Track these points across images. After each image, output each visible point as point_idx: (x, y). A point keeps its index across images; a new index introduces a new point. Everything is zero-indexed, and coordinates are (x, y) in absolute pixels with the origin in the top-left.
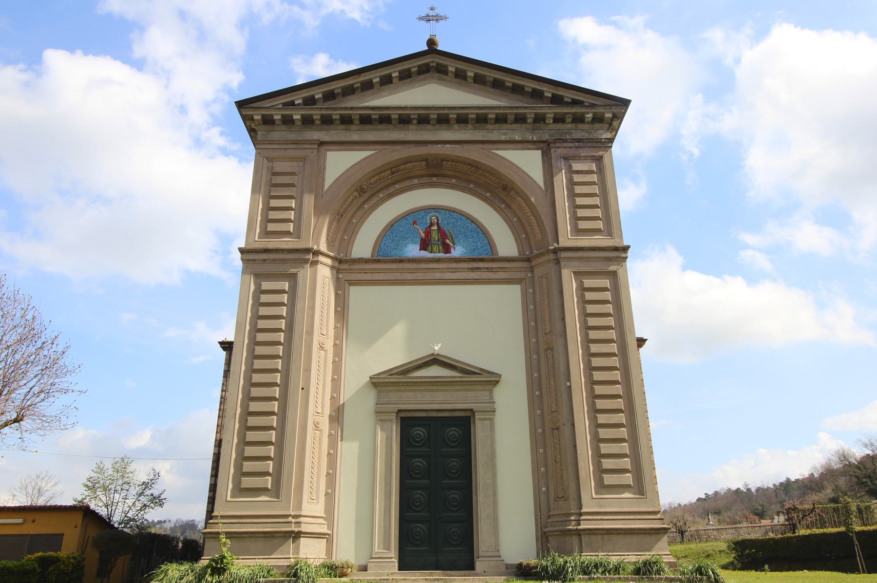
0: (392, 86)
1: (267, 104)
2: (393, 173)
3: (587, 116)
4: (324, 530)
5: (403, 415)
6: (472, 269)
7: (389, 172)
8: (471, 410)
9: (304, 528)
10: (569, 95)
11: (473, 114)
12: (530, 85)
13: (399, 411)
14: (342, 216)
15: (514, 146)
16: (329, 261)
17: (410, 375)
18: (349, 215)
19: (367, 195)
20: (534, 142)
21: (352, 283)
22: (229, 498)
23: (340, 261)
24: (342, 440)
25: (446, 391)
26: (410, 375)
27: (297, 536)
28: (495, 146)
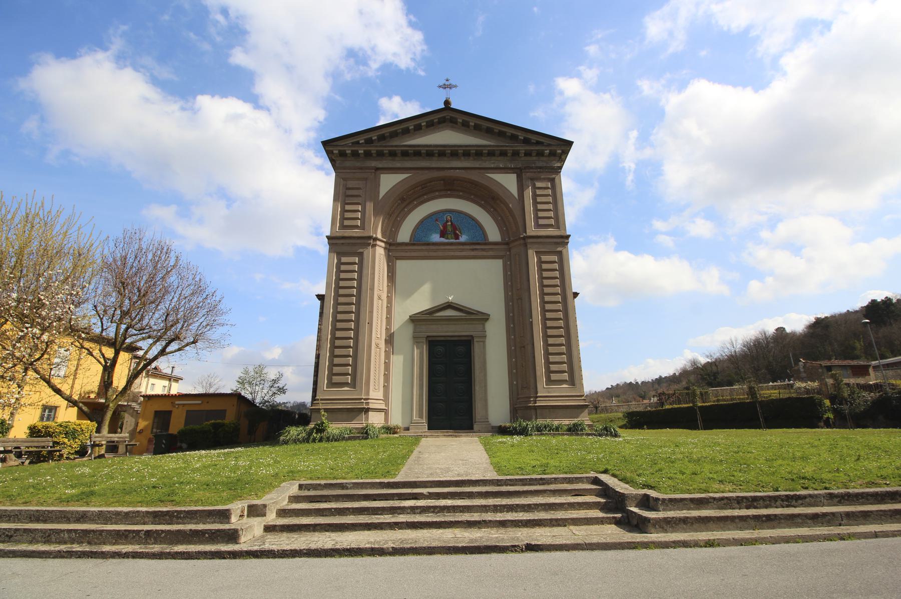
2: (423, 188)
3: (546, 152)
4: (384, 408)
5: (430, 339)
6: (473, 250)
9: (371, 406)
10: (534, 138)
13: (428, 337)
16: (383, 244)
22: (325, 389)
24: (393, 354)
25: (448, 324)
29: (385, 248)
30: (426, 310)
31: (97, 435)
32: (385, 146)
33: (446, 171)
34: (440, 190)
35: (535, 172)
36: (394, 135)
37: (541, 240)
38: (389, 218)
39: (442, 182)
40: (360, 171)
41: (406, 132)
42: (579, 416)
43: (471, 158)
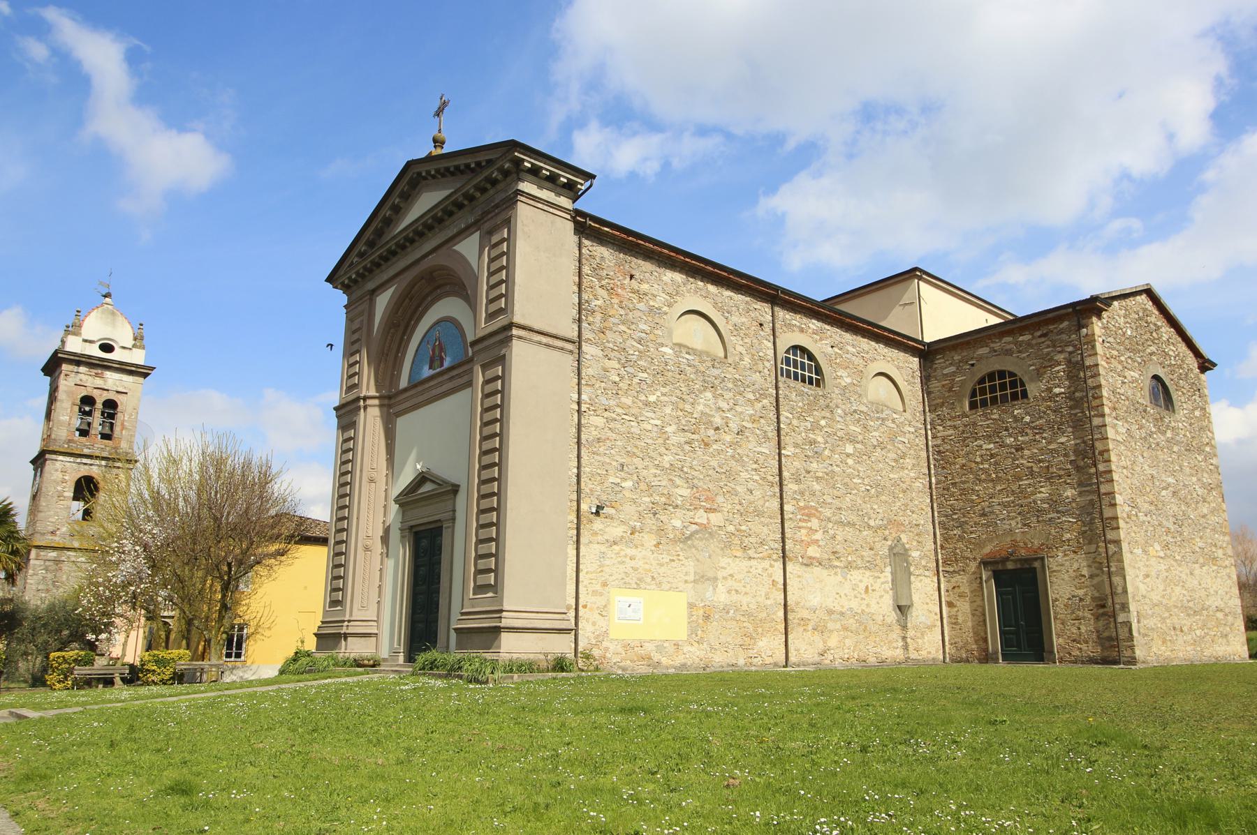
0: (403, 211)
1: (341, 272)
2: (411, 299)
3: (494, 176)
4: (376, 631)
5: (414, 530)
6: (452, 378)
7: (407, 300)
8: (440, 520)
9: (504, 623)
10: (482, 158)
11: (547, 170)
12: (403, 185)
13: (412, 527)
14: (387, 355)
15: (463, 236)
16: (376, 402)
17: (419, 492)
18: (394, 351)
19: (402, 328)
20: (467, 228)
21: (399, 414)
22: (471, 596)
23: (390, 398)
24: (387, 556)
25: (427, 505)
26: (419, 492)
27: (346, 636)
28: (451, 244)
29: (381, 406)
30: (405, 489)
31: (228, 659)
32: (387, 242)
33: (421, 263)
34: (431, 292)
35: (492, 218)
36: (379, 233)
37: (486, 343)
38: (386, 360)
39: (424, 281)
40: (361, 302)
41: (388, 222)
42: (492, 645)
43: (437, 230)
